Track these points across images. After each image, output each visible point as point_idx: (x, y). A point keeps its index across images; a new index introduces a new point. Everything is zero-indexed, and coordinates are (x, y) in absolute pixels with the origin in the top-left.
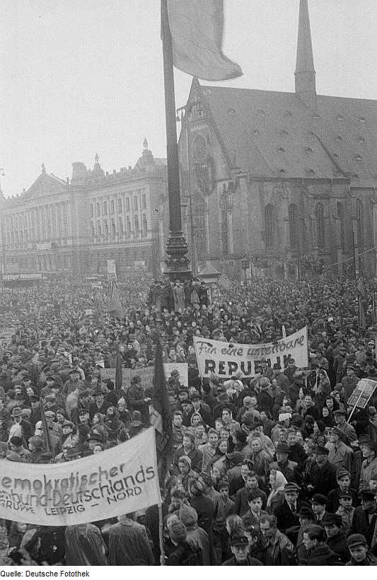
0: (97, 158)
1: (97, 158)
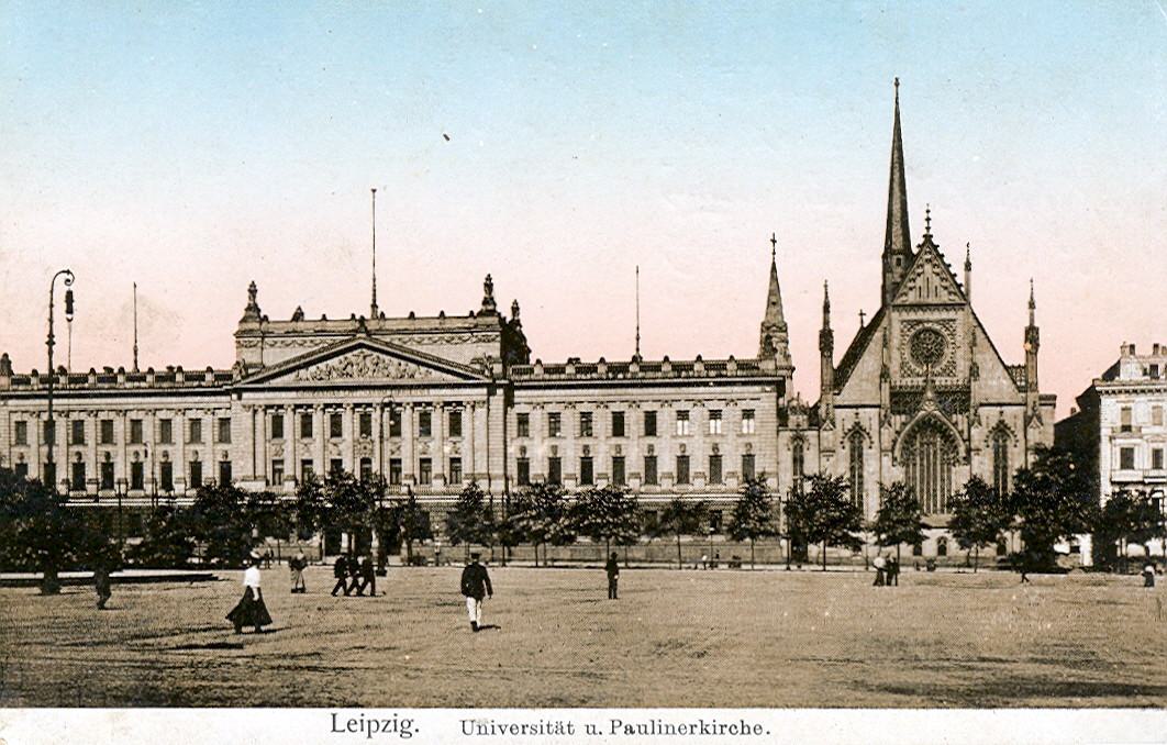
0: (253, 291)
1: (253, 291)
